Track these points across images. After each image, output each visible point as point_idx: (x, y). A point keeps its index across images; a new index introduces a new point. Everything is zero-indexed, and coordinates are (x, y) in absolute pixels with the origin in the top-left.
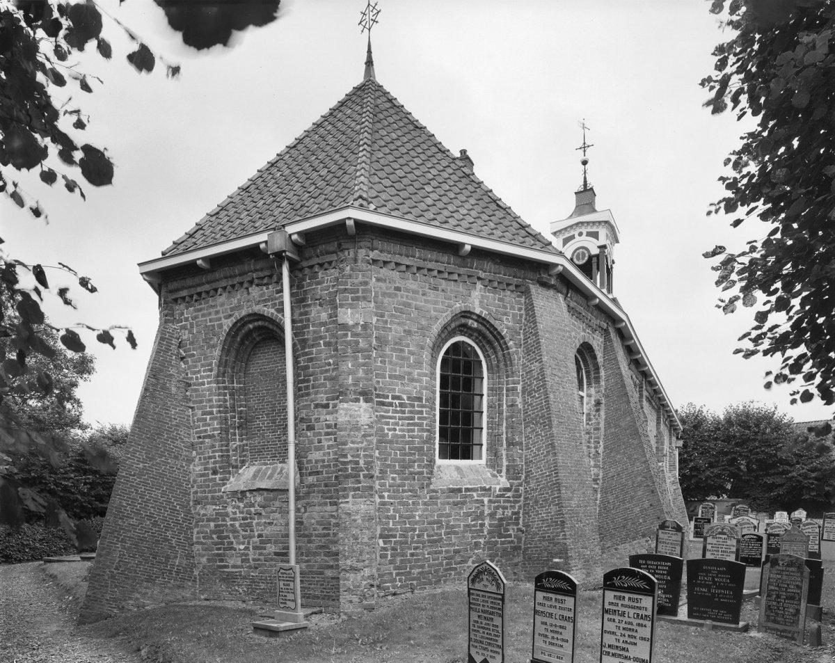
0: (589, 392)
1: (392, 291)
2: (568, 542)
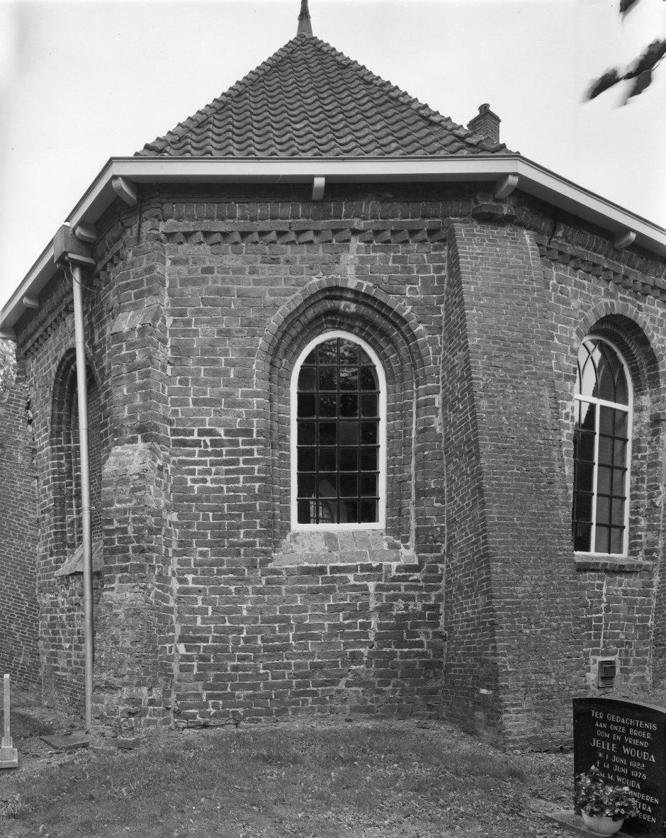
0: (639, 403)
1: (198, 275)
2: (501, 660)
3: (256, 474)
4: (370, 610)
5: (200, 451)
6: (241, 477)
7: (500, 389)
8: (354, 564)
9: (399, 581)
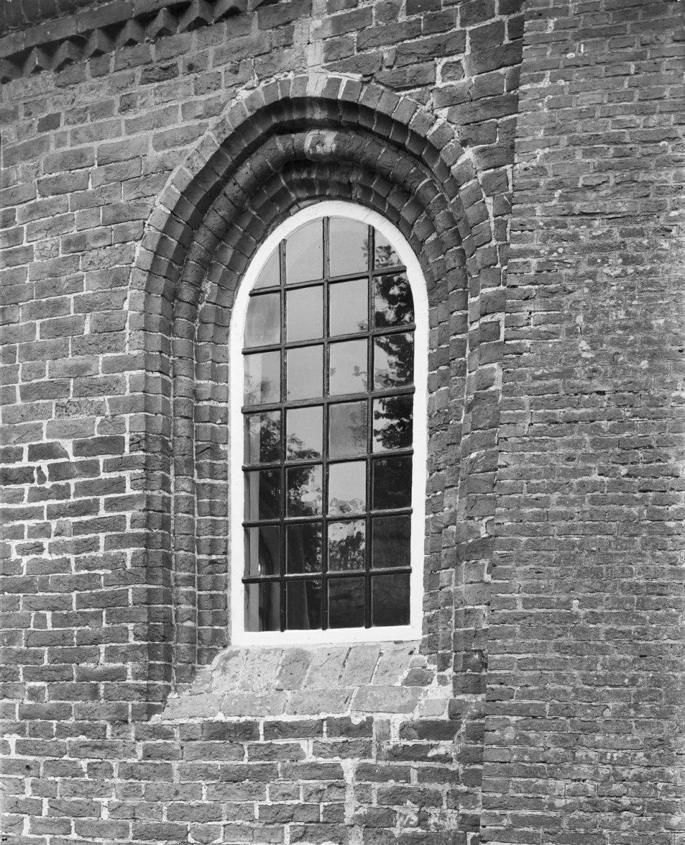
1: (35, 135)
3: (128, 530)
4: (347, 821)
5: (31, 489)
6: (102, 536)
7: (584, 268)
8: (315, 718)
9: (408, 758)
